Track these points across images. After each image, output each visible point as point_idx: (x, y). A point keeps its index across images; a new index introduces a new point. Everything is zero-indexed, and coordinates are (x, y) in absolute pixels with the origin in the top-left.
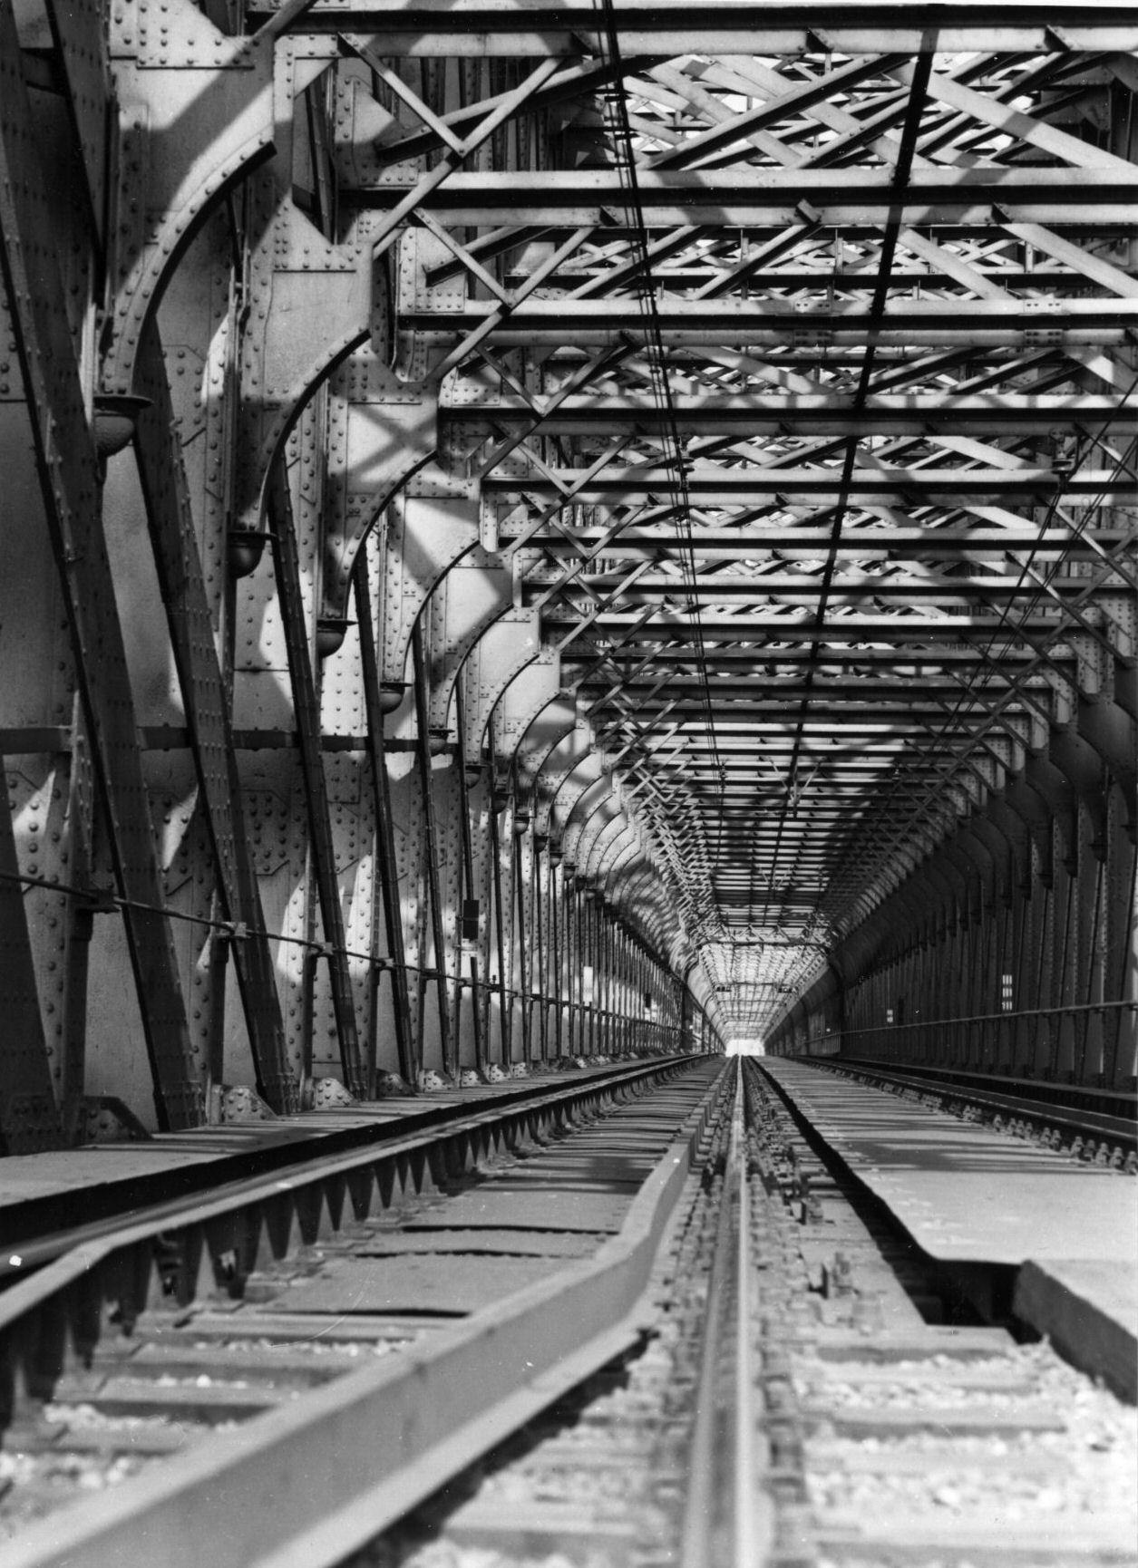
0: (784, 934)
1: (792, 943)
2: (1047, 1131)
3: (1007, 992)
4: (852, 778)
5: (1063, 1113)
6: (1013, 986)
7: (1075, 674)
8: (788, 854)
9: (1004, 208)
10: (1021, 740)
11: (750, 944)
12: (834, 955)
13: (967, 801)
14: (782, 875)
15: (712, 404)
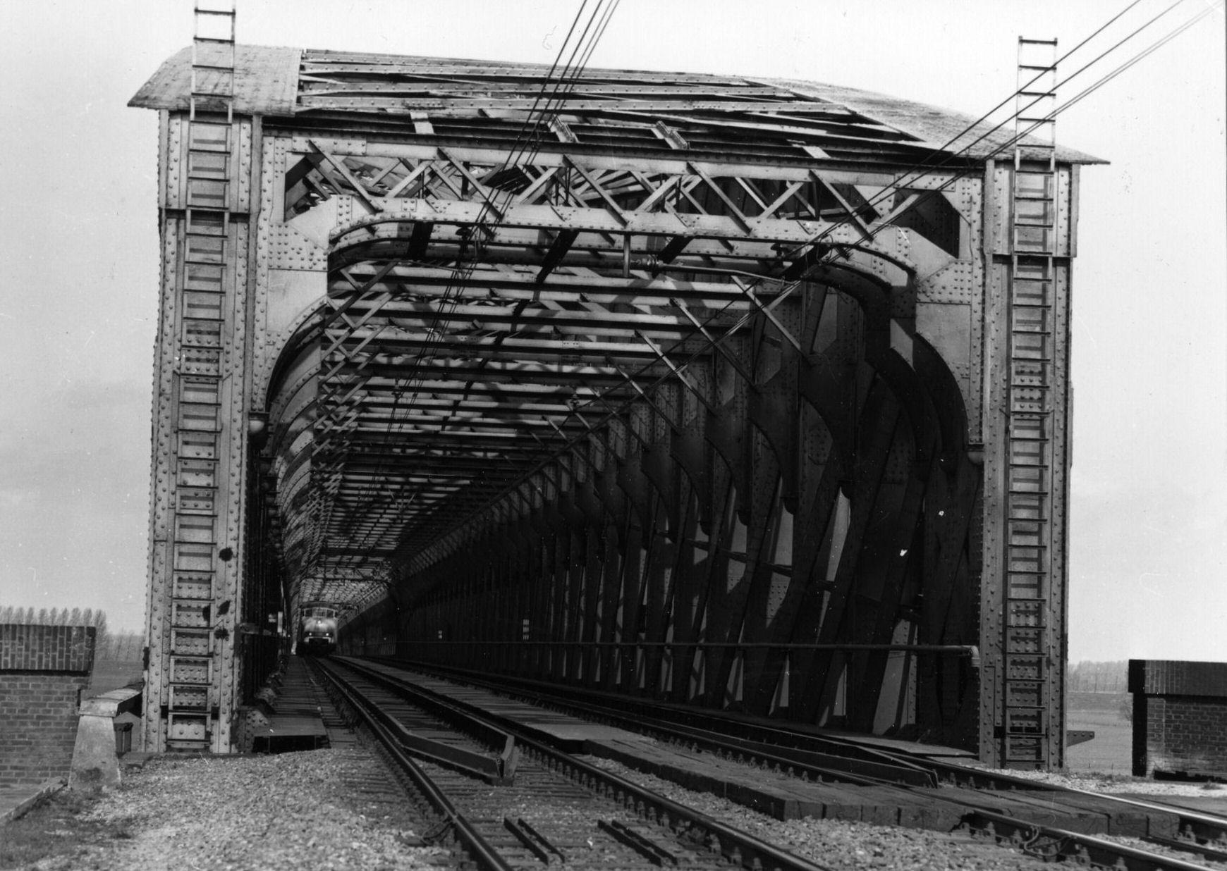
0: (360, 573)
1: (365, 579)
2: (672, 739)
3: (526, 630)
4: (430, 498)
5: (664, 725)
6: (529, 626)
7: (588, 453)
8: (379, 530)
9: (586, 295)
10: (566, 470)
11: (334, 580)
12: (396, 589)
13: (502, 514)
14: (371, 541)
15: (410, 362)
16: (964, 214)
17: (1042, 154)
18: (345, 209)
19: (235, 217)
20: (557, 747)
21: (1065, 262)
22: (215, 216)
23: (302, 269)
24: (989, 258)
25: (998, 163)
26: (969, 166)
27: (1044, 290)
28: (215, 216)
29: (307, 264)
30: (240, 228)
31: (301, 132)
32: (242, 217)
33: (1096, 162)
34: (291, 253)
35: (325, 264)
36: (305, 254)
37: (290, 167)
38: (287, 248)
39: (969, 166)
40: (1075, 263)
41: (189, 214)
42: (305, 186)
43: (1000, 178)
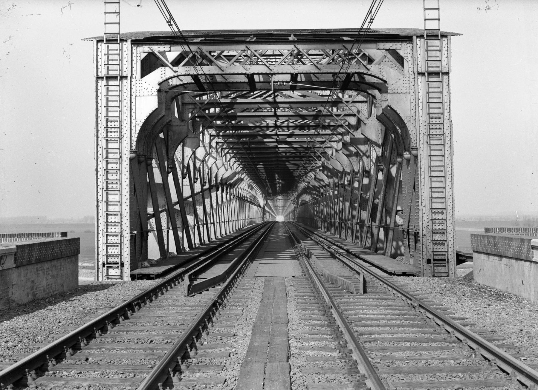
16: (405, 58)
17: (435, 32)
18: (163, 72)
19: (423, 74)
20: (227, 243)
21: (447, 73)
22: (430, 74)
23: (148, 95)
24: (416, 73)
25: (418, 37)
26: (407, 38)
27: (107, 93)
28: (430, 74)
29: (150, 94)
30: (445, 77)
31: (146, 44)
32: (447, 73)
33: (457, 34)
34: (144, 90)
35: (157, 93)
36: (149, 90)
37: (142, 57)
38: (143, 88)
39: (407, 38)
40: (450, 74)
41: (105, 78)
42: (149, 64)
43: (420, 43)
